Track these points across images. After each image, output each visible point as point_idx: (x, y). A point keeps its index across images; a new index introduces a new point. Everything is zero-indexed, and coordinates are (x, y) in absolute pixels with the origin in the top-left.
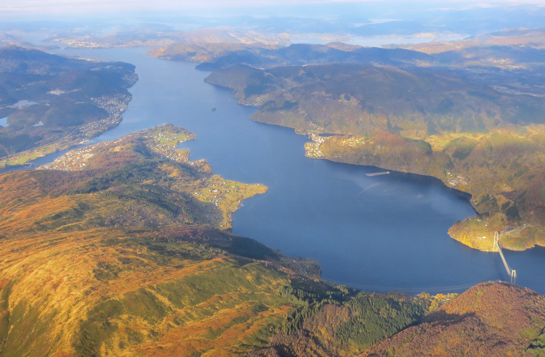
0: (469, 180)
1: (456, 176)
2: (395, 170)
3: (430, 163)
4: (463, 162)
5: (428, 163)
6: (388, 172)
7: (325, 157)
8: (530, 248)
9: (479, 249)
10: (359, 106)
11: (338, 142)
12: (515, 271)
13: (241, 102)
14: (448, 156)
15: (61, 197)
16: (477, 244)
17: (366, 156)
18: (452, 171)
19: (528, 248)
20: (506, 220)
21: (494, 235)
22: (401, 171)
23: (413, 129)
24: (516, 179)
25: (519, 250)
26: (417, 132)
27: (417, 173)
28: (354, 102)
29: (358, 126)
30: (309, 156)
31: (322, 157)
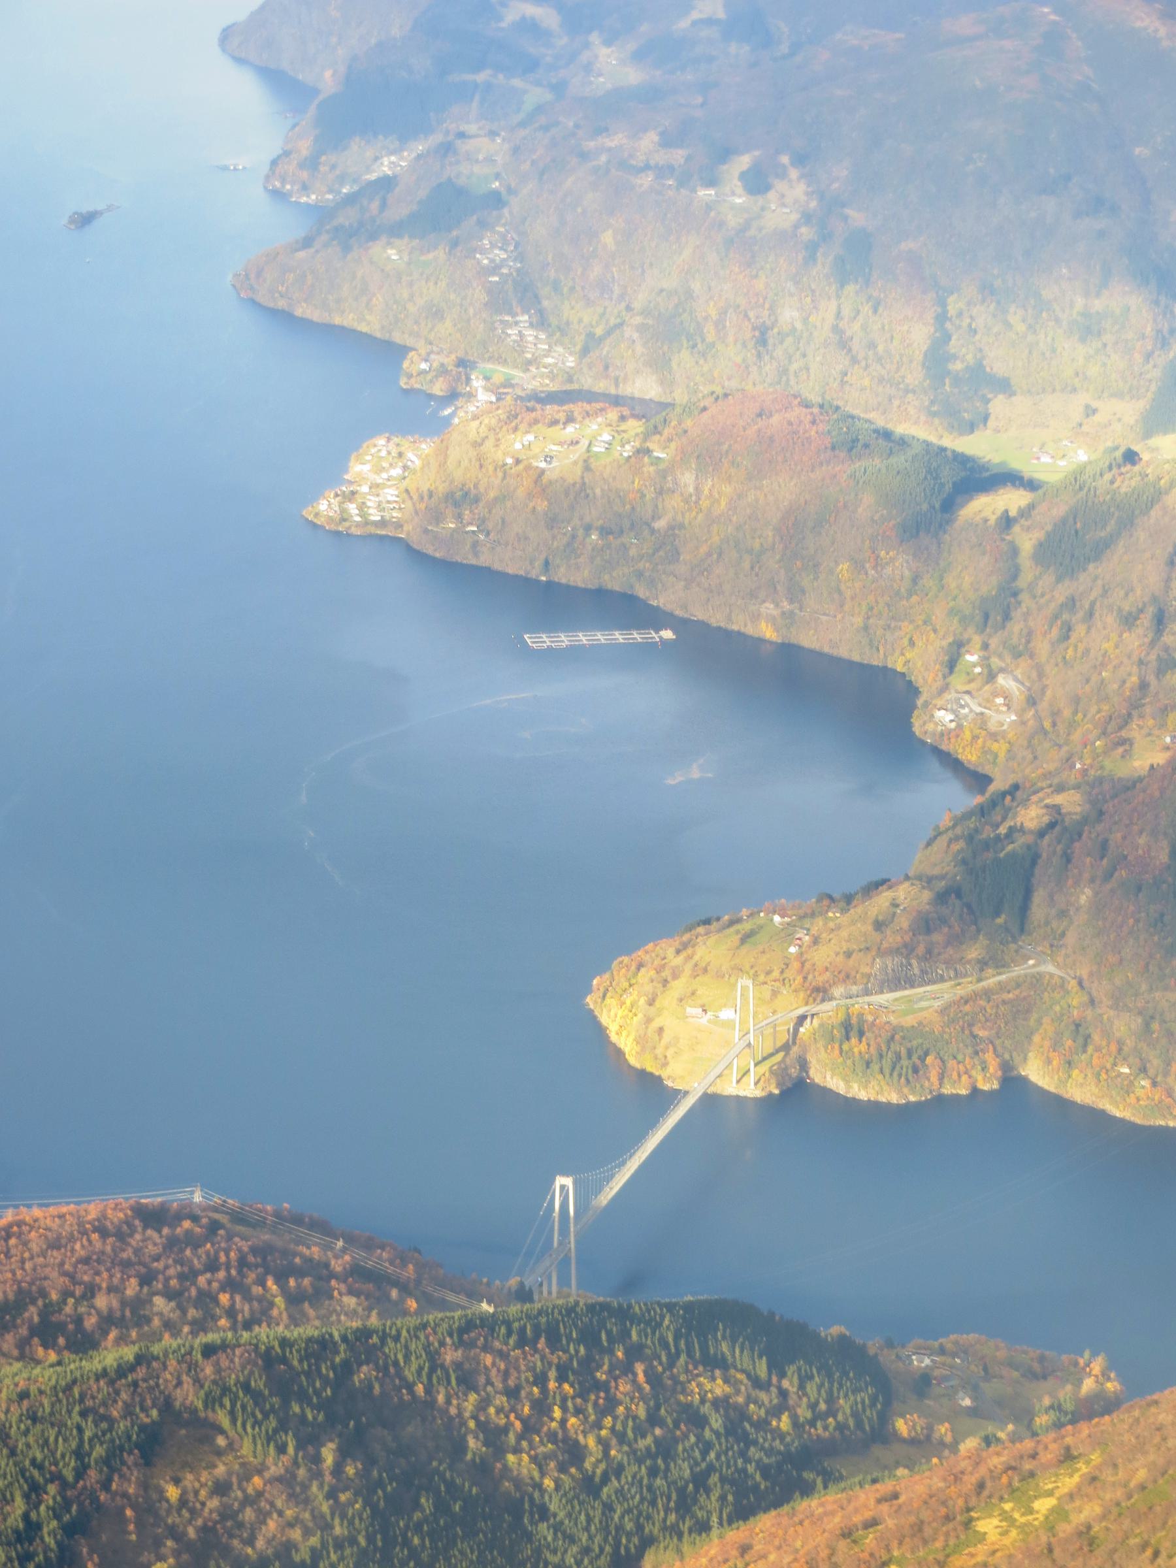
1: (991, 677)
2: (722, 625)
3: (910, 593)
5: (898, 593)
6: (668, 634)
7: (399, 525)
8: (964, 1092)
9: (664, 1073)
10: (804, 230)
11: (489, 444)
12: (568, 1181)
13: (283, 182)
14: (1015, 551)
16: (667, 1048)
17: (605, 532)
18: (994, 642)
19: (947, 1090)
22: (750, 630)
23: (1074, 390)
26: (1090, 411)
27: (826, 650)
28: (784, 205)
30: (317, 515)
31: (383, 523)
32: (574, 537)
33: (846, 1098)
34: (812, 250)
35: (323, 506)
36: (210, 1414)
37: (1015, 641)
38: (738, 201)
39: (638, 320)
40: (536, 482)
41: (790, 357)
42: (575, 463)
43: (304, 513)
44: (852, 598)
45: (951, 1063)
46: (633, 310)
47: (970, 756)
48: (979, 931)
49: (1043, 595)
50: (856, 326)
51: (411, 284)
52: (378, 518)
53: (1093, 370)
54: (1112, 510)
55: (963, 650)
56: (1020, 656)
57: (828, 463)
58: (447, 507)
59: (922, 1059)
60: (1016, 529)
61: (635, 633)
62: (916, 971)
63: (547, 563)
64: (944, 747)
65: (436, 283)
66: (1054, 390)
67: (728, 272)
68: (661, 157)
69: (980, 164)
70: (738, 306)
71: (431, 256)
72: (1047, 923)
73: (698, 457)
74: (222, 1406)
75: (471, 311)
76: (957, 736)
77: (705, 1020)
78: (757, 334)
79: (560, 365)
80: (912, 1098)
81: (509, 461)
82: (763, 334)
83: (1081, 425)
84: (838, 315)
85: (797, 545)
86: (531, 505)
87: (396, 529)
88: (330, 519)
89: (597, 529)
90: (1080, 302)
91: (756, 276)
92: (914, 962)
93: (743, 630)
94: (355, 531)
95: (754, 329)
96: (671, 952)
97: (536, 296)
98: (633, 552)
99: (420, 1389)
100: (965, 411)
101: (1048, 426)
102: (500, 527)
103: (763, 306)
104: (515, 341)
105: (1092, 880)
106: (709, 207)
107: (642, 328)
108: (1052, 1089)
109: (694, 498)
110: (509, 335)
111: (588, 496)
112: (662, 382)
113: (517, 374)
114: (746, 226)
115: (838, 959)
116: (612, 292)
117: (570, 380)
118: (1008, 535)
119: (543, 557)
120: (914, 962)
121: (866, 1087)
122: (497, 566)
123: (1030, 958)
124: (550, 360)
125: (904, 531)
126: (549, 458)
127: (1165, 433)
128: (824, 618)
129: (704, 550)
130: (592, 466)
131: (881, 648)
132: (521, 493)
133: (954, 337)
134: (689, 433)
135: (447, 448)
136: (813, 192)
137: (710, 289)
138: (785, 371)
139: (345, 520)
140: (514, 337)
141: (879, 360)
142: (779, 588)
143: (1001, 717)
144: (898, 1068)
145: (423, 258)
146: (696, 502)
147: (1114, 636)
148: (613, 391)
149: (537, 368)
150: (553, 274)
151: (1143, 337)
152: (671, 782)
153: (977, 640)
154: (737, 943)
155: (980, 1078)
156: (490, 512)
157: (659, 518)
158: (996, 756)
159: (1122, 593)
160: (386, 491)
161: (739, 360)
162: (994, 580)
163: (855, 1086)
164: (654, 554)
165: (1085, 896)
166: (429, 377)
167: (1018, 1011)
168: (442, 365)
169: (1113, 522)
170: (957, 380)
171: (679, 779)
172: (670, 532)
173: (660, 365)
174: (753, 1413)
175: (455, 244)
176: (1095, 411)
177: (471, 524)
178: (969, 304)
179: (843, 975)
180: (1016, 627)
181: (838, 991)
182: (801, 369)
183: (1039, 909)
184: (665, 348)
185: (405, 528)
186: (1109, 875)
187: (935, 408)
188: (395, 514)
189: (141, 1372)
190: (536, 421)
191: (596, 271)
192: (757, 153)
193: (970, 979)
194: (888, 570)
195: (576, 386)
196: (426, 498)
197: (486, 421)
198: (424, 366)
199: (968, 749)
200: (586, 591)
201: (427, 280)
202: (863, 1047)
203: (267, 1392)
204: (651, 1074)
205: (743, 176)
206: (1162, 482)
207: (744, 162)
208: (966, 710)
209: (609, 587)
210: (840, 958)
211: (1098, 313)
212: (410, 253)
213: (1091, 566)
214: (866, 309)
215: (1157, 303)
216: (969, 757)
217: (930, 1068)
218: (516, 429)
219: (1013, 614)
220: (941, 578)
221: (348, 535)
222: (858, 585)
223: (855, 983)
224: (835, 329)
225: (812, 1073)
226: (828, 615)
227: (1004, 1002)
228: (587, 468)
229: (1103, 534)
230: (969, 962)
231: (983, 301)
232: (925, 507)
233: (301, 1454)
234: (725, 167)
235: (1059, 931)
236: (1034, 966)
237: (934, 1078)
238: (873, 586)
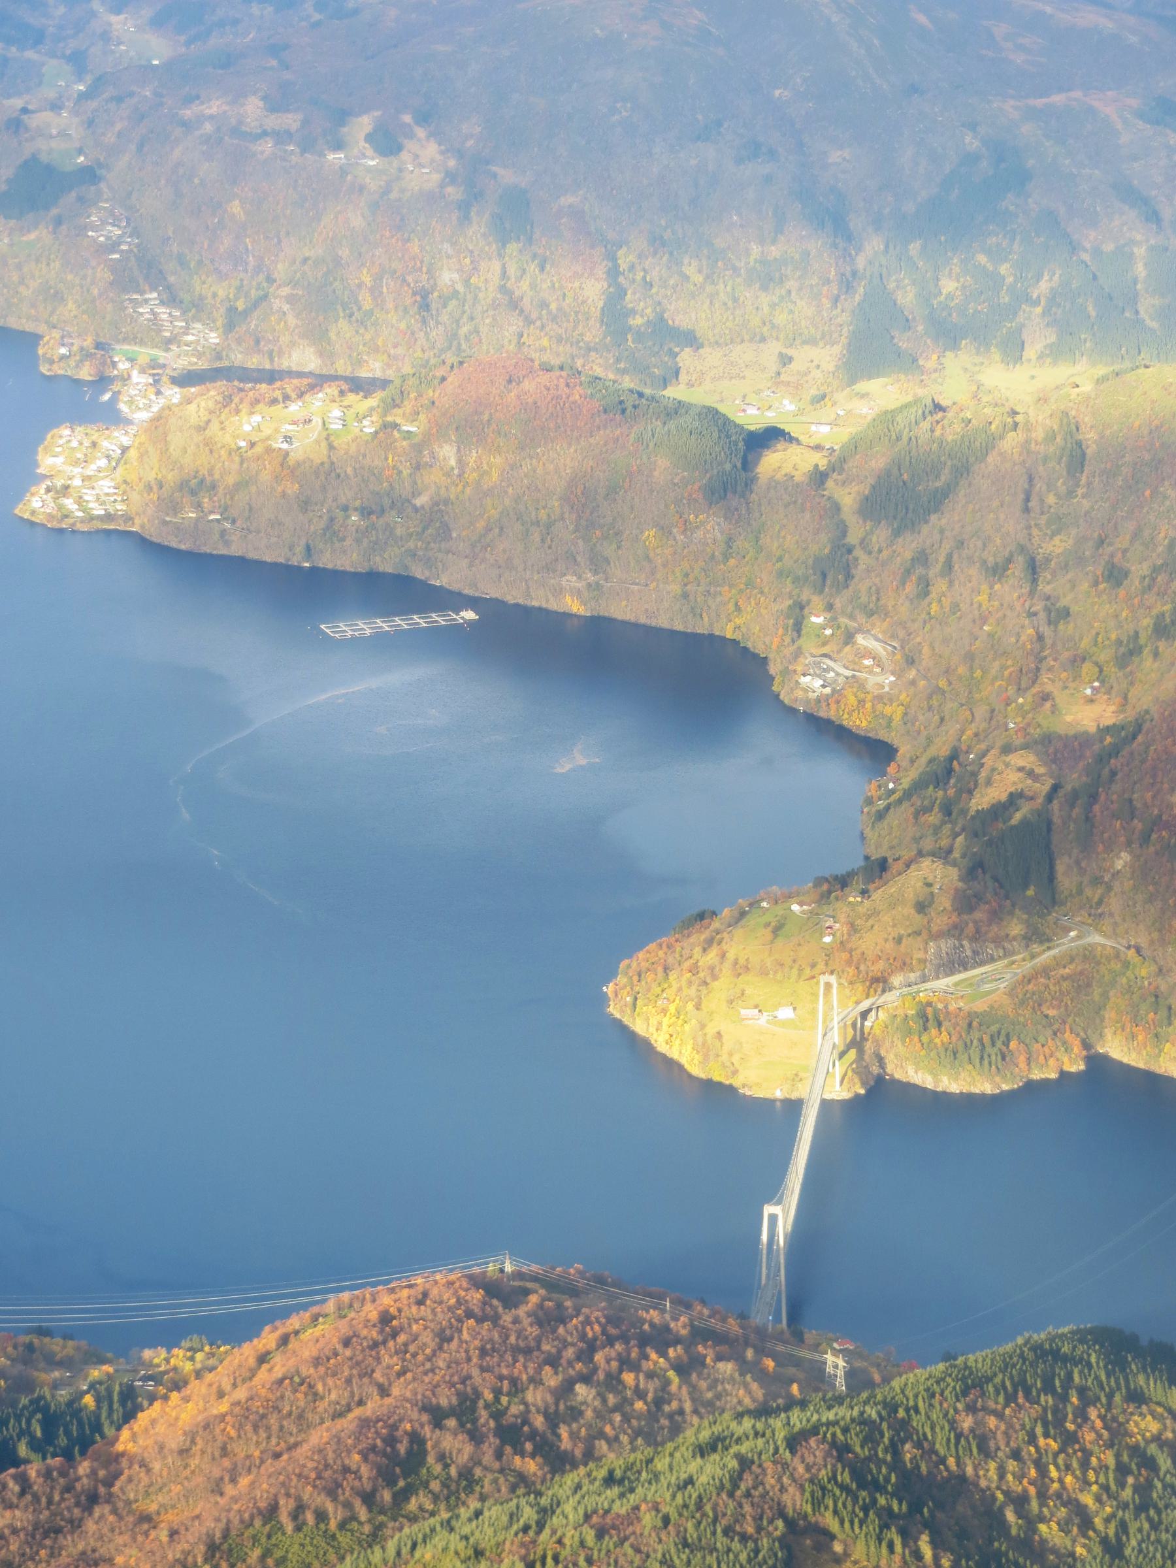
0: (911, 661)
1: (849, 638)
2: (521, 601)
3: (726, 557)
4: (907, 547)
5: (713, 556)
6: (469, 615)
7: (128, 518)
8: (1053, 1076)
9: (736, 1082)
10: (450, 190)
11: (215, 426)
14: (837, 508)
15: (1004, 797)
16: (730, 1054)
17: (366, 512)
18: (838, 603)
19: (1037, 1075)
20: (945, 902)
21: (815, 995)
22: (553, 605)
23: (763, 340)
24: (1156, 654)
25: (976, 1090)
26: (786, 360)
27: (643, 620)
28: (421, 166)
29: (424, 321)
30: (33, 513)
31: (109, 517)
32: (332, 519)
33: (935, 1093)
34: (464, 208)
35: (36, 503)
36: (820, 1519)
37: (864, 599)
38: (372, 163)
39: (286, 291)
40: (282, 465)
41: (457, 321)
42: (318, 442)
43: (17, 511)
44: (665, 565)
45: (1036, 1047)
46: (275, 281)
47: (859, 722)
48: (1013, 905)
49: (880, 551)
50: (525, 285)
51: (19, 267)
52: (103, 512)
53: (781, 318)
54: (943, 458)
55: (806, 611)
56: (872, 615)
57: (605, 427)
58: (183, 497)
59: (1006, 1044)
60: (830, 483)
61: (433, 615)
62: (969, 953)
63: (308, 548)
64: (822, 714)
65: (48, 264)
66: (742, 341)
67: (378, 236)
68: (273, 122)
69: (624, 114)
70: (395, 272)
71: (32, 236)
72: (1080, 892)
73: (457, 428)
74: (826, 1508)
75: (96, 291)
76: (838, 702)
77: (764, 1019)
78: (418, 298)
79: (202, 341)
80: (1005, 1087)
81: (243, 444)
82: (424, 297)
83: (779, 374)
84: (504, 274)
85: (592, 513)
86: (280, 489)
87: (125, 522)
88: (50, 517)
89: (356, 509)
90: (755, 250)
91: (408, 240)
92: (965, 943)
93: (544, 605)
94: (80, 527)
95: (414, 294)
96: (697, 950)
97: (161, 272)
98: (399, 531)
99: (951, 1462)
100: (655, 366)
101: (744, 378)
102: (247, 514)
103: (420, 269)
104: (149, 320)
105: (1129, 843)
106: (343, 171)
107: (290, 299)
108: (1141, 1065)
109: (456, 472)
110: (142, 314)
111: (339, 476)
112: (321, 354)
113: (161, 355)
114: (387, 191)
115: (887, 946)
116: (247, 264)
117: (219, 357)
118: (824, 490)
119: (303, 542)
120: (965, 943)
121: (956, 1080)
122: (252, 555)
123: (1070, 930)
124: (190, 338)
125: (713, 494)
126: (288, 439)
127: (870, 378)
128: (636, 588)
129: (480, 525)
130: (335, 444)
131: (704, 615)
132: (265, 477)
133: (629, 292)
134: (437, 404)
135: (165, 435)
136: (448, 151)
137: (360, 254)
138: (455, 336)
139: (66, 516)
140: (147, 316)
141: (554, 319)
142: (579, 559)
143: (879, 679)
144: (986, 1056)
145: (24, 238)
146: (460, 476)
147: (985, 587)
148: (268, 366)
149: (179, 347)
150: (175, 248)
151: (828, 281)
152: (559, 770)
153: (817, 601)
154: (769, 936)
155: (1066, 1059)
156: (232, 499)
157: (420, 494)
158: (890, 719)
159: (980, 544)
160: (101, 483)
161: (403, 326)
162: (824, 537)
163: (945, 1079)
164: (423, 532)
165: (1122, 861)
166: (72, 363)
167: (1079, 986)
168: (82, 349)
169: (946, 471)
170: (639, 336)
171: (568, 767)
172: (436, 508)
173: (317, 336)
174: (584, 1403)
175: (58, 221)
176: (791, 359)
177: (211, 512)
178: (640, 257)
179: (898, 964)
180: (862, 585)
181: (897, 980)
182: (470, 333)
183: (1066, 880)
184: (321, 318)
185: (137, 521)
186: (1145, 839)
187: (622, 365)
188: (119, 507)
189: (747, 1482)
190: (257, 401)
191: (226, 242)
192: (377, 113)
193: (1021, 956)
194: (699, 534)
195: (226, 363)
196: (155, 489)
197: (203, 404)
198: (63, 351)
199: (855, 714)
200: (356, 575)
201: (38, 261)
202: (945, 1037)
203: (854, 1486)
204: (720, 1084)
205: (369, 138)
206: (993, 427)
207: (364, 124)
208: (832, 674)
209: (381, 569)
210: (890, 946)
211: (776, 259)
212: (9, 235)
213: (933, 518)
214: (533, 268)
215: (835, 246)
216: (858, 722)
217: (1017, 1054)
218: (238, 411)
219: (853, 571)
220: (757, 539)
221: (74, 532)
222: (668, 551)
223: (912, 970)
224: (503, 289)
225: (889, 1070)
226: (637, 584)
227: (1064, 978)
228: (331, 447)
229: (937, 484)
230: (1014, 938)
231: (655, 253)
232: (728, 467)
233: (907, 1552)
234: (345, 130)
235: (1096, 899)
236: (1078, 937)
237: (1023, 1065)
238: (686, 551)
